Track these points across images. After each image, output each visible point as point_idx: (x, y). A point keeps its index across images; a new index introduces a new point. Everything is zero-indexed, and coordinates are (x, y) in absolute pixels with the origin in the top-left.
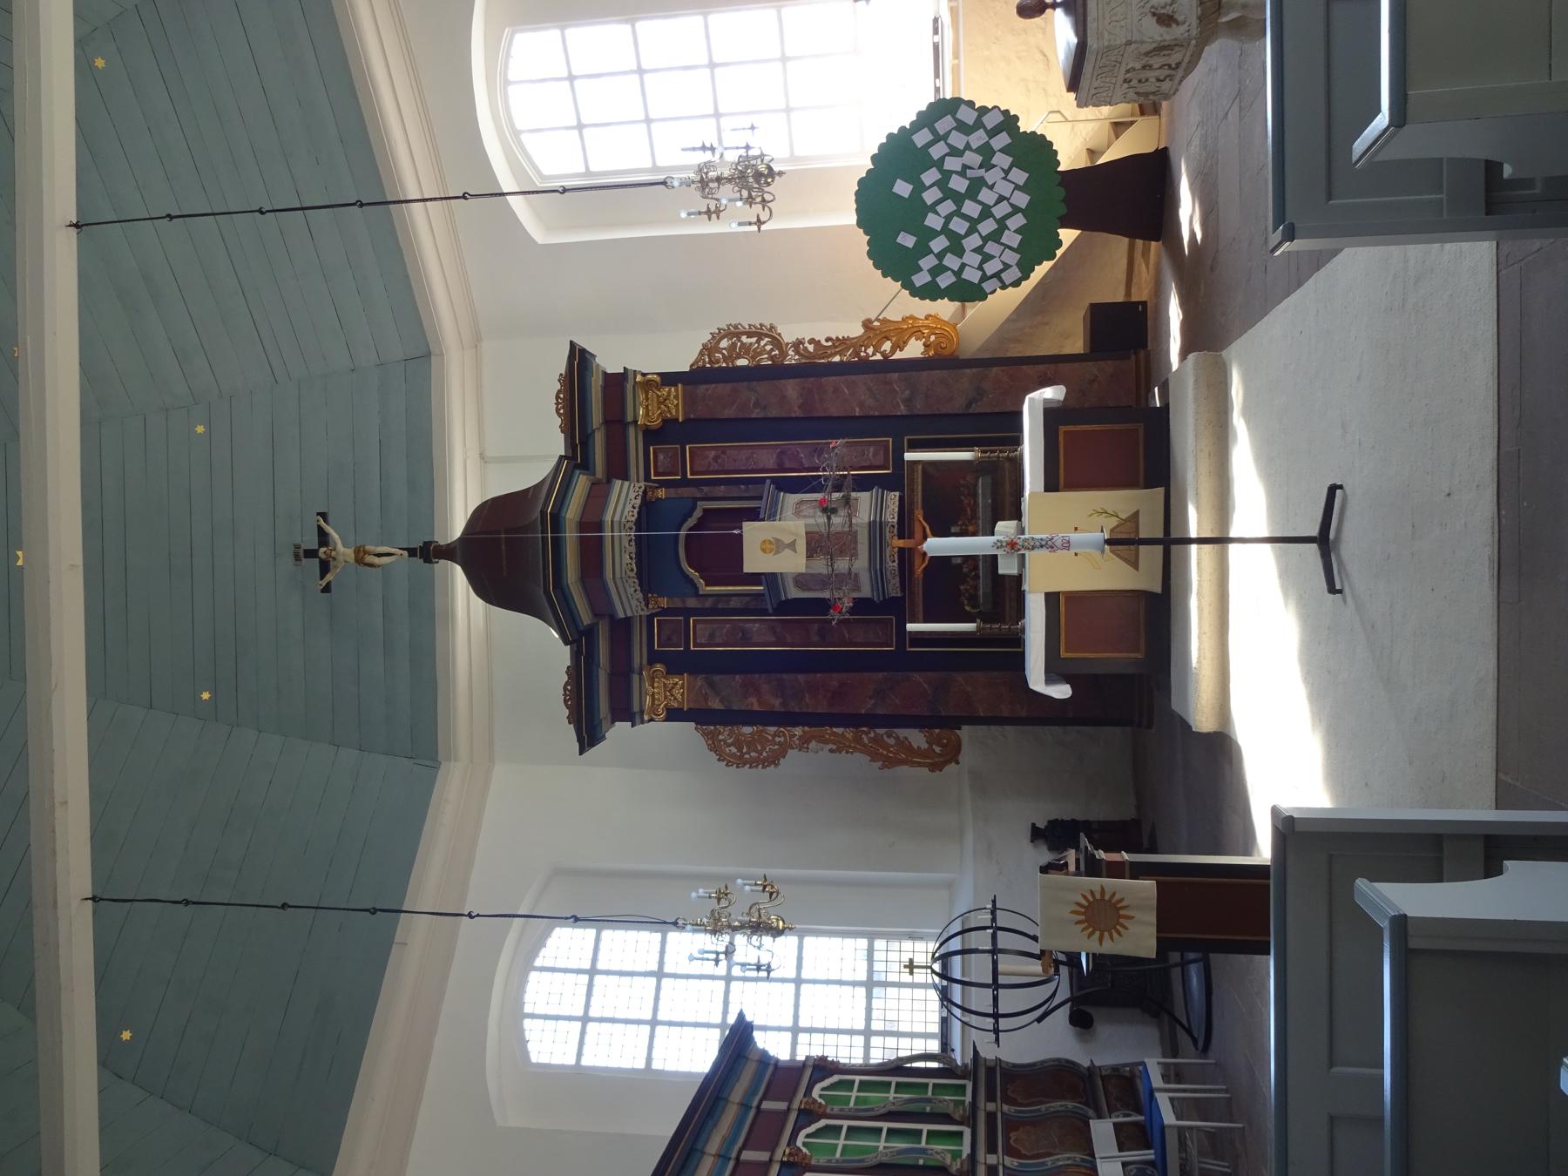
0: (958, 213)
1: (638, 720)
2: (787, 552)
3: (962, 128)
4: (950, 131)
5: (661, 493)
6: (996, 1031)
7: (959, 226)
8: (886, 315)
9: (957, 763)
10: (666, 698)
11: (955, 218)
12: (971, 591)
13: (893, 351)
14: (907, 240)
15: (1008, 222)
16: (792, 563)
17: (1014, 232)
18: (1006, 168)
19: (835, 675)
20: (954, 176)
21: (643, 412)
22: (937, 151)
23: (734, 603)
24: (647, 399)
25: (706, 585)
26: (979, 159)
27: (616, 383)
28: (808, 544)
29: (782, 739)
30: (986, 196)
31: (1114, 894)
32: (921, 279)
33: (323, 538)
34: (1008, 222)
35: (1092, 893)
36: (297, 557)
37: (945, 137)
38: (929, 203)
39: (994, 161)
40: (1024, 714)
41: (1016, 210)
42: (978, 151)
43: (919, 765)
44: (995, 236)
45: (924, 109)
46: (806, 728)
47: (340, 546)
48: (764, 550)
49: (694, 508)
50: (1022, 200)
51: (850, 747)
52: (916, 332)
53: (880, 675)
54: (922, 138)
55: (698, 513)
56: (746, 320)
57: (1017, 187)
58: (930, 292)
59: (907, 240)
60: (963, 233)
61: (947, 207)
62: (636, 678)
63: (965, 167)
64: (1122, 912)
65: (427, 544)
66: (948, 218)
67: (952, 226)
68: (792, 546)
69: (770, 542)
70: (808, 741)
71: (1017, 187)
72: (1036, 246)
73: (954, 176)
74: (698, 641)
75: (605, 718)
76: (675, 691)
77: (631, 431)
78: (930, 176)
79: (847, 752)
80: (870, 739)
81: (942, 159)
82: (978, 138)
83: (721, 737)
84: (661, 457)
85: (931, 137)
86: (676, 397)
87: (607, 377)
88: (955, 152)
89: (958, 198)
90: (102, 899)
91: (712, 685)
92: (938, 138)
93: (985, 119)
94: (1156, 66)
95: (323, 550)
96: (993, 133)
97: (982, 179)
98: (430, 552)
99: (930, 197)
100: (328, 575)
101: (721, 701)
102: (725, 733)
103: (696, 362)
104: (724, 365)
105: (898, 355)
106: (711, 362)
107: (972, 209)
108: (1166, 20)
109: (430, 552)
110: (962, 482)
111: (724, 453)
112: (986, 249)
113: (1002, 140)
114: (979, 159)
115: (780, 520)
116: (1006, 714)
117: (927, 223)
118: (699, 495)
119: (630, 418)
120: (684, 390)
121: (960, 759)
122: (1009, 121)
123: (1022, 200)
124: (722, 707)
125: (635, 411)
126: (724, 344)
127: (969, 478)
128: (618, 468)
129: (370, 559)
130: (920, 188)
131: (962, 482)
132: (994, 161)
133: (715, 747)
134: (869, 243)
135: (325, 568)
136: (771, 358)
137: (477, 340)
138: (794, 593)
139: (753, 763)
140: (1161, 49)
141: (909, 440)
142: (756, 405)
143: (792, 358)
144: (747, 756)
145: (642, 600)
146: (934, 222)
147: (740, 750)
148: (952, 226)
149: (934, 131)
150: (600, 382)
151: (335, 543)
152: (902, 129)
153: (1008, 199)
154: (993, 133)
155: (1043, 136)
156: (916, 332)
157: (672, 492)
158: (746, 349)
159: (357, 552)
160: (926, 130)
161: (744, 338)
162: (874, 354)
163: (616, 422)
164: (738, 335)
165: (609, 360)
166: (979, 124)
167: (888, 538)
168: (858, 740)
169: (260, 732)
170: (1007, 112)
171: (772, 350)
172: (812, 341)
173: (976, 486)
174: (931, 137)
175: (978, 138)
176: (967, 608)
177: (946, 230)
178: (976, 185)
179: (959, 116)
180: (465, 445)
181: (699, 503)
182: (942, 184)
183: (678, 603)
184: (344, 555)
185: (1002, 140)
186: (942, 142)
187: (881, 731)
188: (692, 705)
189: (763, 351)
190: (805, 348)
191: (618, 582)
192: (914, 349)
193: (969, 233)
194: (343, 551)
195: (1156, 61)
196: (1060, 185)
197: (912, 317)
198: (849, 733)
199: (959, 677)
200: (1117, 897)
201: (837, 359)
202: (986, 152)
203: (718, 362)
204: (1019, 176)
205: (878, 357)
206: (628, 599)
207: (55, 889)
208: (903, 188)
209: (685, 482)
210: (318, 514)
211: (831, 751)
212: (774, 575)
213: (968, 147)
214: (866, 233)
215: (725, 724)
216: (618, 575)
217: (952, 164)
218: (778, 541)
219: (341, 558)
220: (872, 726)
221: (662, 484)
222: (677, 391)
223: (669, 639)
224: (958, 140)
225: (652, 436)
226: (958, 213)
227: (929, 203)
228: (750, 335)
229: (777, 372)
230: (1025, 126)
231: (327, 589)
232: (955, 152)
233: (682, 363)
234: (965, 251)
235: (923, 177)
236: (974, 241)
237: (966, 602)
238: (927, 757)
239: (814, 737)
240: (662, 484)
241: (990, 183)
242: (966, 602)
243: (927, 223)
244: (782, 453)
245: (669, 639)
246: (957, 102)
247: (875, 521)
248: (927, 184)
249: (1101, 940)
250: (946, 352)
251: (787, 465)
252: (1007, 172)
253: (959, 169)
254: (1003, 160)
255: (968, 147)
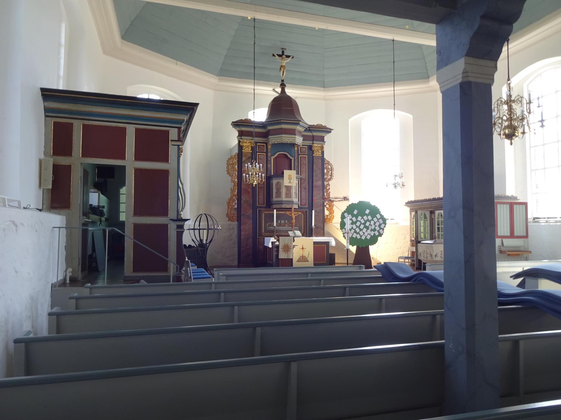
0: (361, 224)
1: (239, 138)
2: (289, 181)
3: (380, 225)
4: (379, 222)
5: (296, 149)
6: (194, 229)
7: (358, 224)
8: (334, 206)
9: (228, 221)
10: (246, 146)
11: (360, 223)
12: (272, 225)
13: (326, 208)
14: (355, 212)
15: (358, 235)
16: (286, 182)
17: (356, 236)
18: (371, 234)
19: (251, 190)
20: (369, 223)
21: (316, 145)
22: (375, 219)
23: (269, 165)
24: (319, 147)
25: (273, 158)
26: (373, 228)
27: (322, 139)
28: (288, 186)
29: (234, 176)
30: (365, 230)
31: (290, 251)
32: (346, 214)
33: (288, 57)
34: (358, 235)
35: (290, 247)
36: (283, 49)
37: (378, 221)
38: (364, 217)
39: (372, 232)
40: (242, 237)
41: (361, 236)
42: (375, 228)
43: (228, 211)
44: (355, 232)
45: (384, 217)
46: (237, 182)
47: (286, 61)
48: (289, 175)
49: (292, 157)
50: (363, 238)
51: (232, 193)
52: (331, 213)
53: (251, 202)
54: (378, 216)
55: (291, 158)
56: (334, 173)
57: (366, 237)
58: (343, 217)
59: (355, 212)
60: (356, 225)
61: (363, 221)
62: (251, 138)
63: (371, 225)
64: (287, 252)
65: (285, 85)
66: (360, 221)
67: (358, 222)
68: (290, 182)
69: (291, 177)
70: (234, 182)
71: (366, 237)
72: (352, 241)
73: (369, 223)
74: (259, 155)
75: (240, 129)
76: (247, 148)
77: (311, 142)
78: (370, 218)
79: (231, 192)
80: (234, 198)
81: (373, 220)
82: (377, 228)
83: (234, 159)
84: (304, 149)
85: (378, 218)
86: (319, 154)
87: (324, 137)
88: (375, 223)
89: (364, 224)
90: (255, 22)
91: (249, 158)
92: (378, 219)
93: (381, 230)
94: (427, 255)
95: (285, 56)
96: (378, 231)
97: (368, 229)
98: (283, 86)
99: (365, 218)
100: (278, 57)
101: (244, 160)
102: (236, 161)
103: (326, 159)
104: (325, 167)
105: (326, 209)
106: (326, 163)
107: (362, 227)
108: (436, 256)
109: (283, 86)
110: (298, 223)
111: (305, 165)
112: (352, 230)
113: (377, 233)
114: (373, 228)
115: (296, 180)
116: (242, 233)
117: (359, 217)
118: (295, 158)
119: (314, 142)
120: (320, 156)
121: (230, 221)
122: (380, 235)
123: (363, 238)
124: (243, 161)
125: (316, 143)
126: (330, 167)
127: (298, 225)
128: (305, 138)
129: (282, 69)
130: (367, 215)
131: (298, 223)
132: (372, 232)
133: (231, 158)
134: (355, 204)
135: (279, 56)
136: (326, 178)
137: (325, 100)
138: (275, 182)
139: (228, 167)
140: (431, 255)
141: (307, 211)
142: (316, 174)
143: (326, 183)
144: (230, 166)
145: (275, 143)
146: (359, 218)
147: (231, 164)
148: (358, 222)
149: (380, 219)
150: (323, 135)
151: (286, 60)
152: (380, 212)
153: (364, 235)
154: (378, 231)
155: (377, 242)
156: (331, 213)
157: (296, 151)
158: (328, 172)
159: (284, 66)
160: (380, 217)
161: (330, 172)
162: (326, 203)
163: (313, 138)
164: (331, 170)
165: (327, 137)
166: (380, 228)
167: (280, 205)
168: (234, 195)
169: (236, 30)
170: (382, 234)
171: (328, 178)
172: (329, 188)
173: (296, 226)
174: (378, 218)
175: (377, 228)
176: (268, 224)
177: (357, 221)
178: (367, 228)
179: (383, 224)
180: (301, 94)
181: (293, 158)
182: (368, 220)
183: (269, 151)
184: (284, 63)
185: (377, 233)
186: (383, 222)
187: (236, 201)
188: (243, 153)
189: (327, 176)
190: (328, 187)
191: (281, 138)
192: (327, 213)
193: (356, 226)
194: (285, 62)
195: (428, 255)
196: (366, 246)
197: (334, 212)
198: (236, 193)
199: (251, 222)
200: (290, 251)
201: (325, 194)
202: (374, 230)
203: (326, 165)
204: (369, 237)
205: (325, 204)
206: (273, 139)
207: (260, 12)
208: (367, 211)
209: (298, 155)
210: (293, 56)
211: (231, 188)
212: (283, 176)
213: (376, 226)
214: (358, 203)
215: (238, 161)
216: (283, 138)
217: (372, 222)
218: (291, 179)
219: (283, 62)
220: (238, 199)
221: (298, 149)
222: (320, 154)
223: (260, 148)
224: (377, 224)
225: (310, 148)
226: (361, 224)
227: (364, 217)
228: (331, 173)
229: (323, 180)
230: (379, 238)
231: (274, 55)
232: (375, 223)
233: (326, 156)
234: (378, 226)
235: (370, 216)
236: (354, 227)
237: (269, 224)
238: (230, 213)
239: (235, 184)
240: (298, 149)
241: (367, 231)
242: (269, 224)
243: (359, 217)
244: (305, 180)
245: (260, 148)
246: (385, 224)
247: (294, 202)
248: (368, 217)
249: (282, 248)
250: (326, 220)
251: (302, 181)
252: (370, 234)
253: (371, 224)
254: (372, 233)
255: (376, 226)
